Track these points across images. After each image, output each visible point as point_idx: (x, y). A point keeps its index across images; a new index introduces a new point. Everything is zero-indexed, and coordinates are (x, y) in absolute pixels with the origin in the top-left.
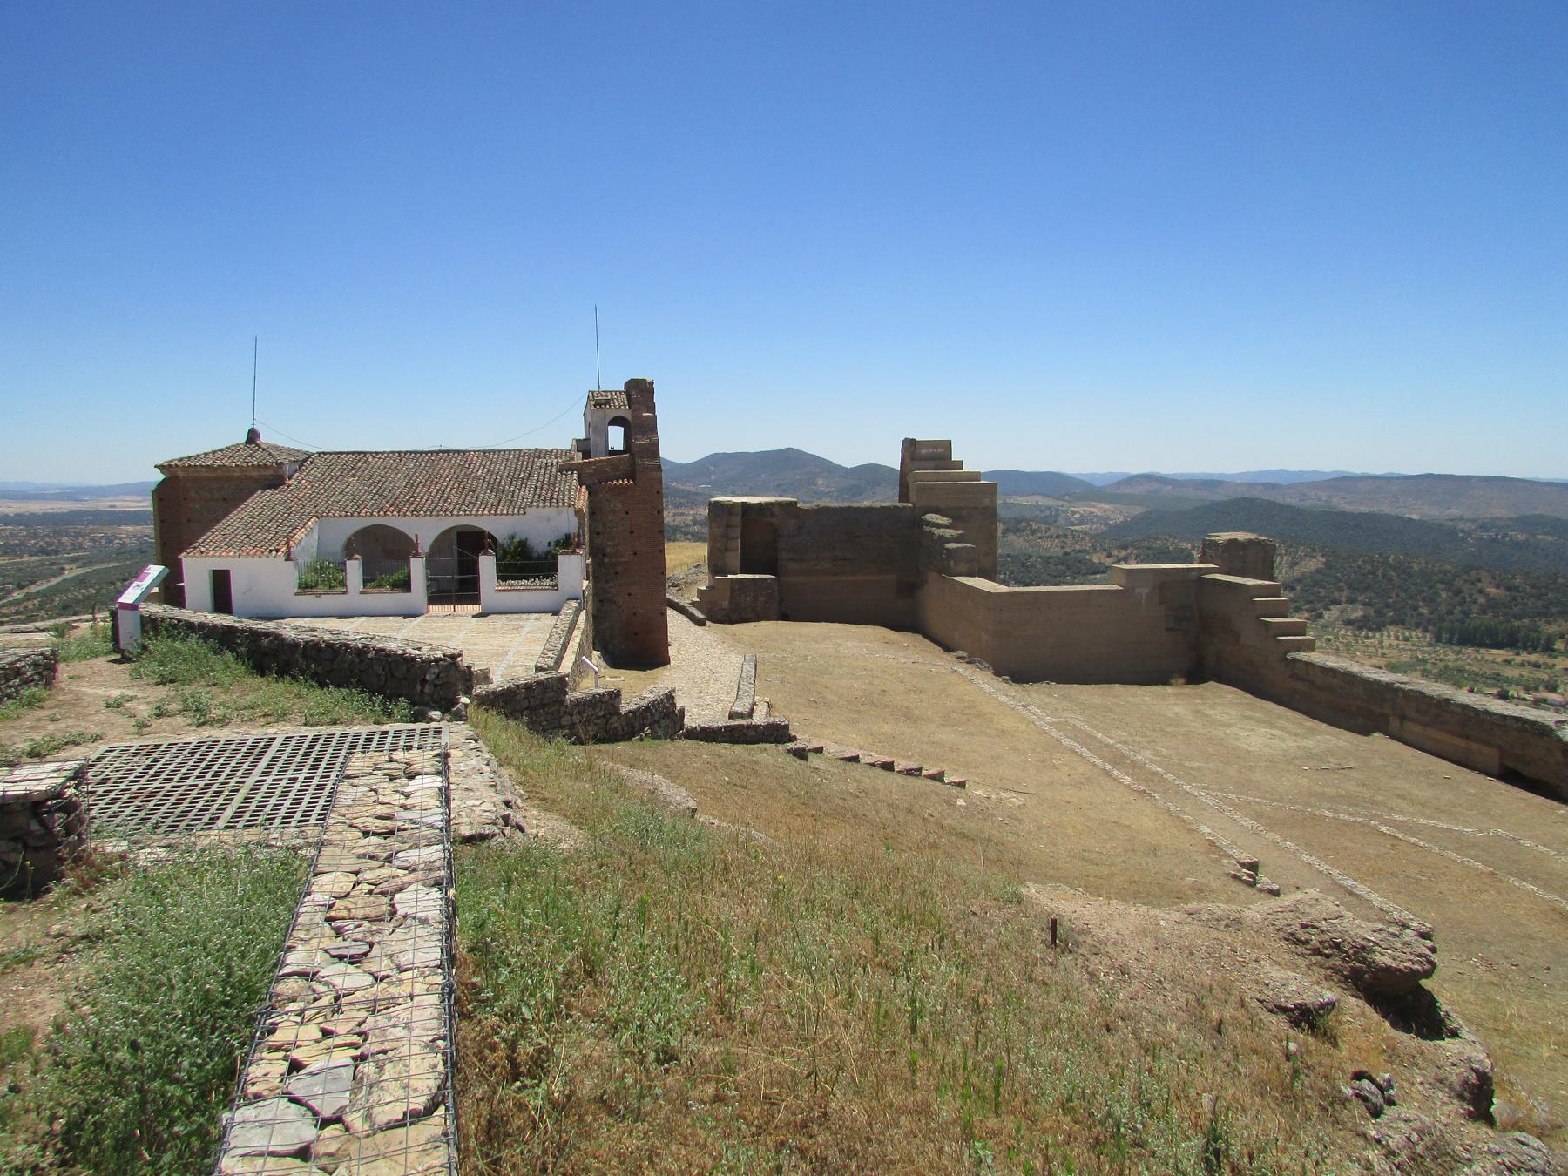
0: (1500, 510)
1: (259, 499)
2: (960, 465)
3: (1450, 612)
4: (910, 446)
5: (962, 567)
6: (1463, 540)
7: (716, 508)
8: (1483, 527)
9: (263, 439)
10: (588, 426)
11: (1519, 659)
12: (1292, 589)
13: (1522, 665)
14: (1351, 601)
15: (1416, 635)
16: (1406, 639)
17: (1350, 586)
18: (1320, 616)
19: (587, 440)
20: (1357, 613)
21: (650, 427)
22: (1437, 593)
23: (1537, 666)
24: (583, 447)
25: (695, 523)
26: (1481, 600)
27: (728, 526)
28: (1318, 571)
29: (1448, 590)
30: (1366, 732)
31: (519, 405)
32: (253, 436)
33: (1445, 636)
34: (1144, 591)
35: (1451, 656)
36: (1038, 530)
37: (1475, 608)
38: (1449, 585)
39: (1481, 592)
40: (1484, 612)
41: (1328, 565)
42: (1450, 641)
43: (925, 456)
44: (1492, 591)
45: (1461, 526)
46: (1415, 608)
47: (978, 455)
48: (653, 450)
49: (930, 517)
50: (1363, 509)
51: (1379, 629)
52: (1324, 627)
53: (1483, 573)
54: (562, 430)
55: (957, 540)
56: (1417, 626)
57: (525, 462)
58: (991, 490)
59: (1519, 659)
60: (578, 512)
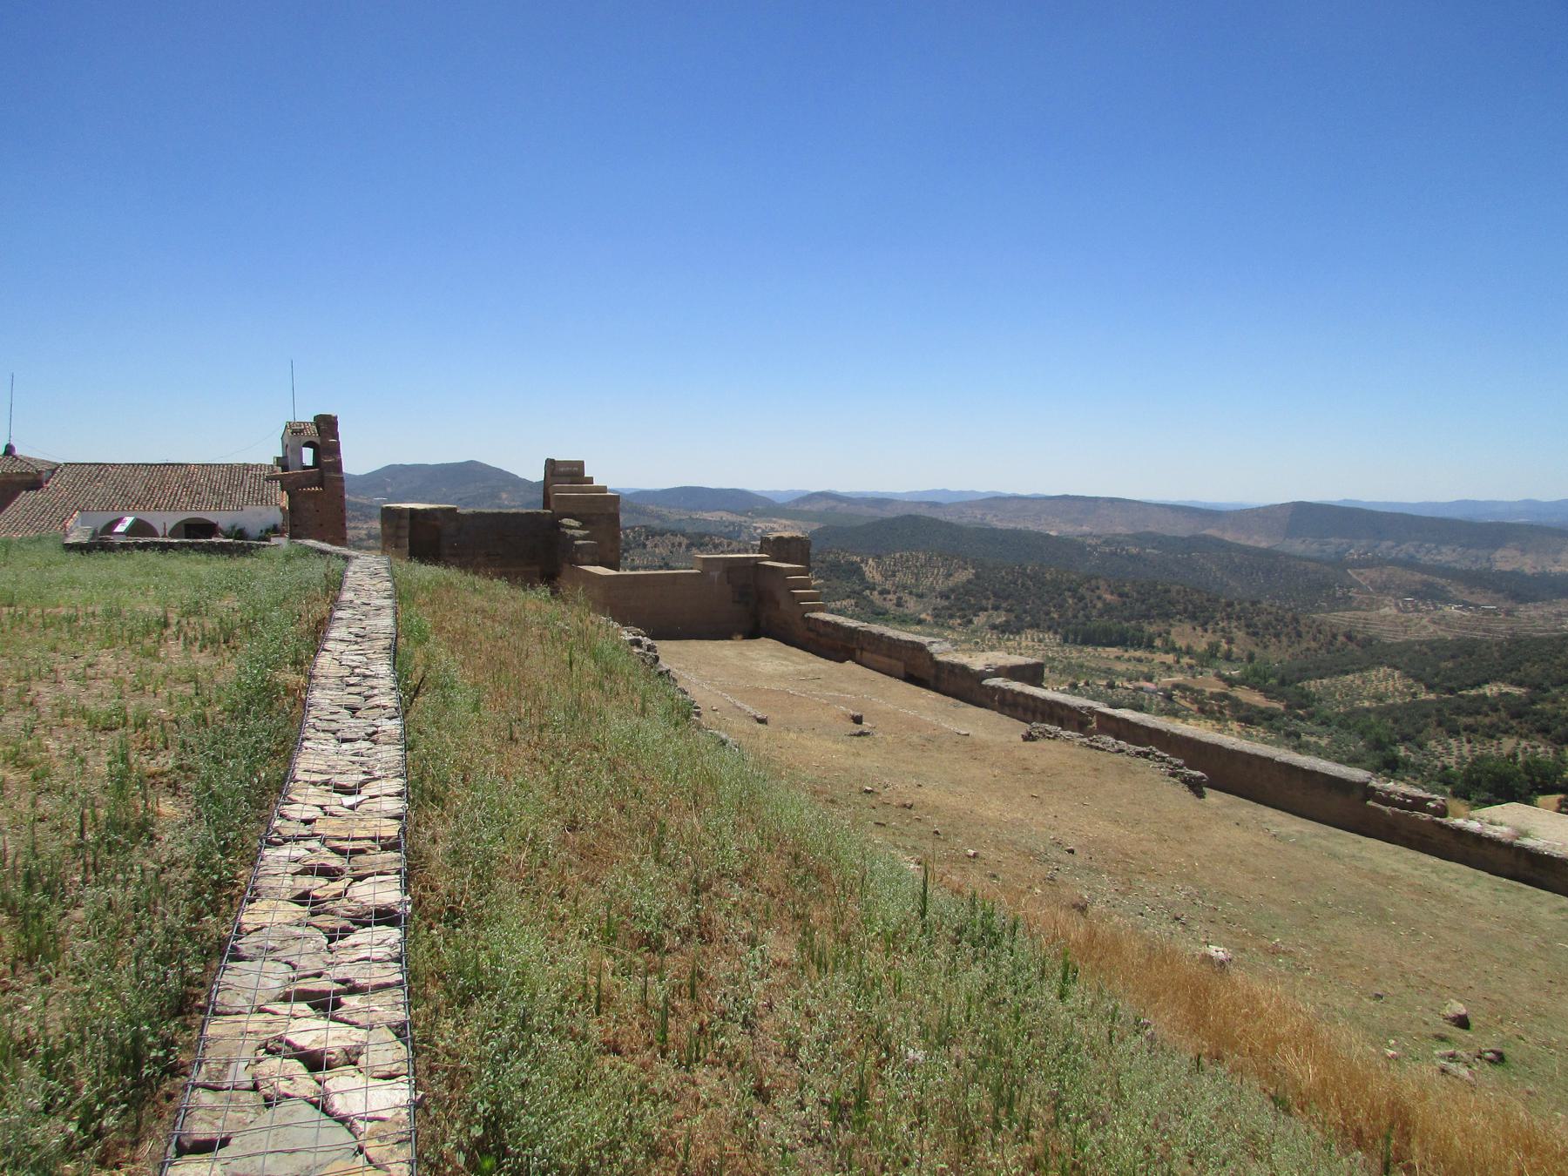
0: (1121, 527)
1: (25, 498)
2: (590, 480)
3: (1075, 617)
4: (551, 464)
5: (586, 559)
6: (1090, 553)
7: (389, 515)
8: (1107, 543)
9: (17, 452)
10: (285, 447)
11: (1126, 655)
12: (948, 598)
13: (1129, 660)
14: (996, 608)
15: (1049, 637)
16: (1040, 641)
17: (995, 595)
18: (971, 622)
19: (285, 457)
20: (1000, 618)
21: (335, 450)
22: (1065, 600)
23: (1140, 660)
24: (282, 462)
25: (369, 536)
26: (1099, 605)
27: (398, 527)
28: (969, 582)
29: (1073, 597)
30: (842, 661)
31: (240, 432)
32: (9, 450)
33: (1071, 637)
34: (715, 574)
35: (1075, 654)
36: (721, 544)
37: (1095, 612)
38: (1074, 591)
39: (1099, 598)
40: (1101, 615)
41: (977, 576)
42: (1075, 642)
43: (563, 473)
44: (1108, 597)
45: (1089, 541)
46: (1048, 613)
47: (612, 472)
48: (338, 466)
49: (565, 521)
50: (1012, 526)
51: (1018, 633)
52: (974, 631)
53: (1102, 583)
54: (265, 450)
55: (583, 538)
56: (1049, 628)
57: (237, 475)
58: (615, 499)
59: (1126, 655)
60: (282, 509)
